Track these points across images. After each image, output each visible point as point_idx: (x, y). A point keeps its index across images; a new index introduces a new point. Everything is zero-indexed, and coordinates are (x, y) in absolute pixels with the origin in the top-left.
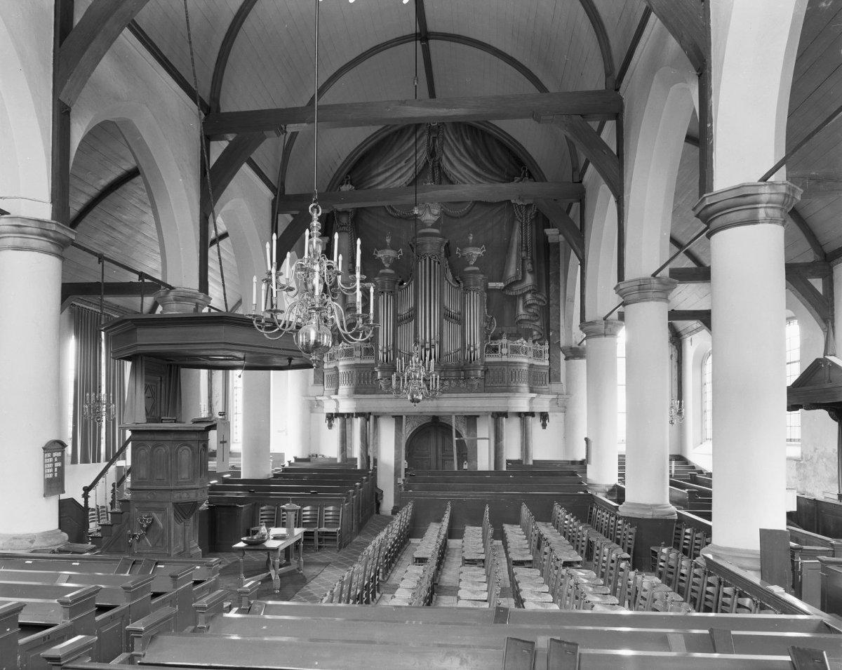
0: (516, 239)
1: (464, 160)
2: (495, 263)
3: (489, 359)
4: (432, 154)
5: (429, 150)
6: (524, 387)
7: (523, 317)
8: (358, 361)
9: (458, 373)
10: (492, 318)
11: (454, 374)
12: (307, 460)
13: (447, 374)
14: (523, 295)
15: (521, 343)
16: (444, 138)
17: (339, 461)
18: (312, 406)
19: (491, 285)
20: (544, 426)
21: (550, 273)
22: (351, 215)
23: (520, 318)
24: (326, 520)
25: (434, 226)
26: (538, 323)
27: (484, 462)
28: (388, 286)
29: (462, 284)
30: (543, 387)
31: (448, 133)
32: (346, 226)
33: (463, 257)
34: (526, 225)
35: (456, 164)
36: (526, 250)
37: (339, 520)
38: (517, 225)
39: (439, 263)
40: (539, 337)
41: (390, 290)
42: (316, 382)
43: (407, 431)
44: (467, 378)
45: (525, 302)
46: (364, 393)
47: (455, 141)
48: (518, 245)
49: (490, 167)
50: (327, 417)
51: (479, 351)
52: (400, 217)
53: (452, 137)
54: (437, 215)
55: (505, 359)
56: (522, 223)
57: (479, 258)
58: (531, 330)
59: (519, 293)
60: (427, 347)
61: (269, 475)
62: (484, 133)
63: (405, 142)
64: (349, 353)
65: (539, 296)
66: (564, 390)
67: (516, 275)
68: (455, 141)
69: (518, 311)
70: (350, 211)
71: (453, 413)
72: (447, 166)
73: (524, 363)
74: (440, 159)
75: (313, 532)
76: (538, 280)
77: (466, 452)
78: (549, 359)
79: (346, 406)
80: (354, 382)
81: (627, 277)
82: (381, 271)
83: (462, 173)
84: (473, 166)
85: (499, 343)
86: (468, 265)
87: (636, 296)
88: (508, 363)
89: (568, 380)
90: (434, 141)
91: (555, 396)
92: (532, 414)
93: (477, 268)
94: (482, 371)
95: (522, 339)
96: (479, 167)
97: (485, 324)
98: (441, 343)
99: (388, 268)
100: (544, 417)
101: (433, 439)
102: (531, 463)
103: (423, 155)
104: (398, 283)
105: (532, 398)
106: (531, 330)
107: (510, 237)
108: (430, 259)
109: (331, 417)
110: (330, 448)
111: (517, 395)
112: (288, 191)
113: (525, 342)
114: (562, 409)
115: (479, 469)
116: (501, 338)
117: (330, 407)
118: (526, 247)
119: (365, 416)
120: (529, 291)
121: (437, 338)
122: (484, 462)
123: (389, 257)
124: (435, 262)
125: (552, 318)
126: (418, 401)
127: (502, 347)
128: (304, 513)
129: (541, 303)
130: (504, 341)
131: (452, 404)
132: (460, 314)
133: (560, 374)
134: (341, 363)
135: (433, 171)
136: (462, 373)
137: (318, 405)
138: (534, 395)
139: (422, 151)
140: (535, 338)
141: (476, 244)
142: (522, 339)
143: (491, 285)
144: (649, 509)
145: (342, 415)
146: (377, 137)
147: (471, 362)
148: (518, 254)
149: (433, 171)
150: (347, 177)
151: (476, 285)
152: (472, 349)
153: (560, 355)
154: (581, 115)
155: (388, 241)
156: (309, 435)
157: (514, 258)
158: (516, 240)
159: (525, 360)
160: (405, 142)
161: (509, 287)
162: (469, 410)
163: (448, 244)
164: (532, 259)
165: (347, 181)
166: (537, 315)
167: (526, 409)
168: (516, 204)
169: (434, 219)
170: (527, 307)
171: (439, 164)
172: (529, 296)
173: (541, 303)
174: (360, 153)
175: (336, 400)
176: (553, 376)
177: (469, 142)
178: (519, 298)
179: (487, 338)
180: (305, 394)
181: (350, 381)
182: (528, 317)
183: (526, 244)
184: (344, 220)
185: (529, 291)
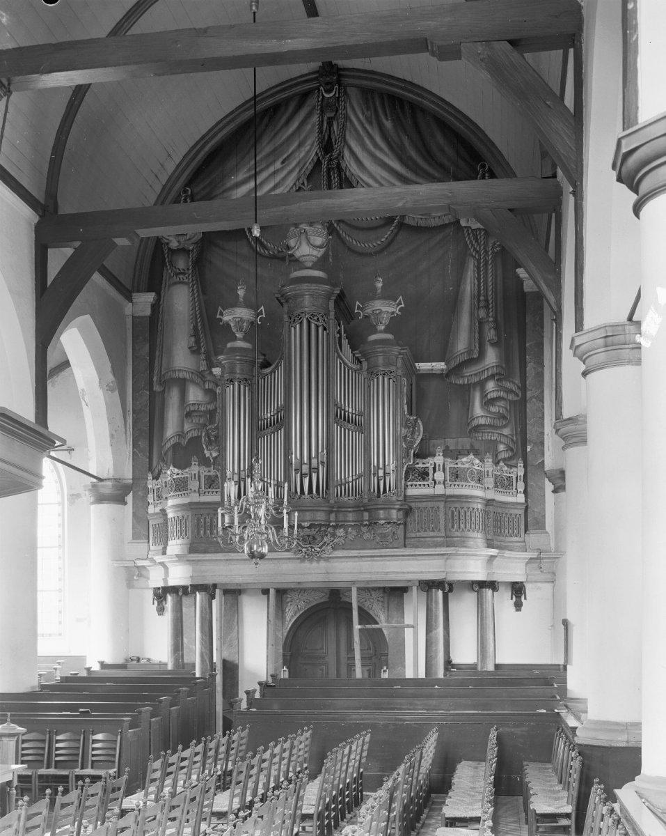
0: (468, 287)
1: (378, 154)
2: (423, 328)
3: (411, 492)
4: (327, 146)
5: (321, 141)
6: (477, 538)
7: (482, 421)
8: (195, 498)
9: (333, 512)
10: (416, 421)
11: (351, 517)
12: (123, 667)
13: (341, 517)
14: (482, 384)
15: (468, 462)
16: (346, 118)
17: (170, 667)
18: (131, 575)
19: (424, 366)
20: (518, 606)
21: (527, 345)
22: (193, 256)
23: (476, 422)
24: (93, 755)
25: (315, 266)
26: (506, 431)
27: (413, 665)
28: (242, 370)
29: (365, 365)
30: (515, 539)
31: (353, 109)
32: (185, 274)
33: (366, 317)
34: (486, 264)
35: (368, 162)
36: (487, 307)
37: (114, 755)
38: (471, 265)
39: (325, 329)
40: (509, 454)
41: (246, 376)
42: (136, 536)
43: (291, 615)
44: (373, 523)
45: (484, 395)
46: (205, 552)
47: (364, 122)
48: (473, 297)
49: (426, 167)
50: (155, 594)
51: (393, 477)
52: (274, 257)
53: (361, 116)
54: (321, 247)
55: (439, 490)
56: (478, 261)
57: (393, 319)
58: (495, 443)
59: (476, 380)
60: (304, 471)
61: (35, 687)
62: (414, 108)
63: (282, 127)
64: (181, 486)
65: (509, 385)
66: (552, 545)
67: (470, 351)
68: (364, 122)
69: (472, 410)
70: (191, 248)
71: (354, 582)
72: (353, 168)
73: (477, 497)
74: (341, 155)
75: (67, 777)
76: (506, 359)
77: (380, 650)
78: (525, 492)
79: (179, 575)
80: (189, 533)
81: (588, 323)
82: (229, 345)
83: (378, 178)
84: (397, 166)
85: (429, 463)
86: (375, 331)
87: (601, 357)
88: (446, 498)
89: (559, 529)
90: (330, 124)
91: (535, 555)
92: (493, 585)
93: (389, 336)
94: (399, 510)
95: (471, 456)
96: (411, 170)
97: (404, 431)
98: (329, 465)
99: (240, 340)
100: (518, 590)
101: (331, 632)
102: (491, 668)
103: (308, 150)
104: (257, 366)
105: (492, 557)
106: (495, 443)
107: (459, 282)
108: (309, 323)
109: (161, 594)
110: (157, 648)
111: (462, 551)
112: (66, 208)
113: (477, 461)
114: (549, 577)
115: (407, 677)
116: (434, 455)
117: (156, 579)
118: (487, 301)
119: (208, 590)
120: (492, 377)
121: (323, 456)
122: (413, 665)
123: (242, 320)
124: (317, 327)
125: (530, 421)
126: (262, 556)
127: (434, 470)
128: (58, 745)
129: (511, 397)
130: (439, 460)
131: (350, 567)
132: (361, 414)
133: (544, 516)
134: (170, 502)
135: (329, 177)
136: (366, 515)
137: (140, 575)
138: (493, 552)
139: (309, 142)
140: (501, 456)
141: (389, 296)
142: (471, 456)
143: (424, 366)
144: (622, 731)
145: (174, 590)
146: (233, 120)
147: (379, 496)
148: (472, 314)
149: (329, 177)
150: (185, 191)
151: (388, 364)
152: (381, 473)
153: (544, 483)
154: (512, 42)
155: (241, 293)
156: (124, 620)
157: (465, 320)
158: (468, 288)
159: (478, 493)
160: (282, 127)
161: (457, 370)
162: (379, 577)
163: (341, 297)
164: (496, 321)
165: (186, 196)
166: (504, 417)
167: (481, 577)
168: (470, 227)
169: (315, 253)
170: (487, 403)
171: (339, 165)
172: (491, 385)
173: (511, 397)
174: (207, 149)
175: (162, 564)
176: (530, 520)
177: (388, 124)
178: (474, 390)
179: (408, 455)
180: (117, 555)
181: (183, 533)
182: (488, 421)
183: (486, 296)
184: (181, 263)
185: (492, 377)
